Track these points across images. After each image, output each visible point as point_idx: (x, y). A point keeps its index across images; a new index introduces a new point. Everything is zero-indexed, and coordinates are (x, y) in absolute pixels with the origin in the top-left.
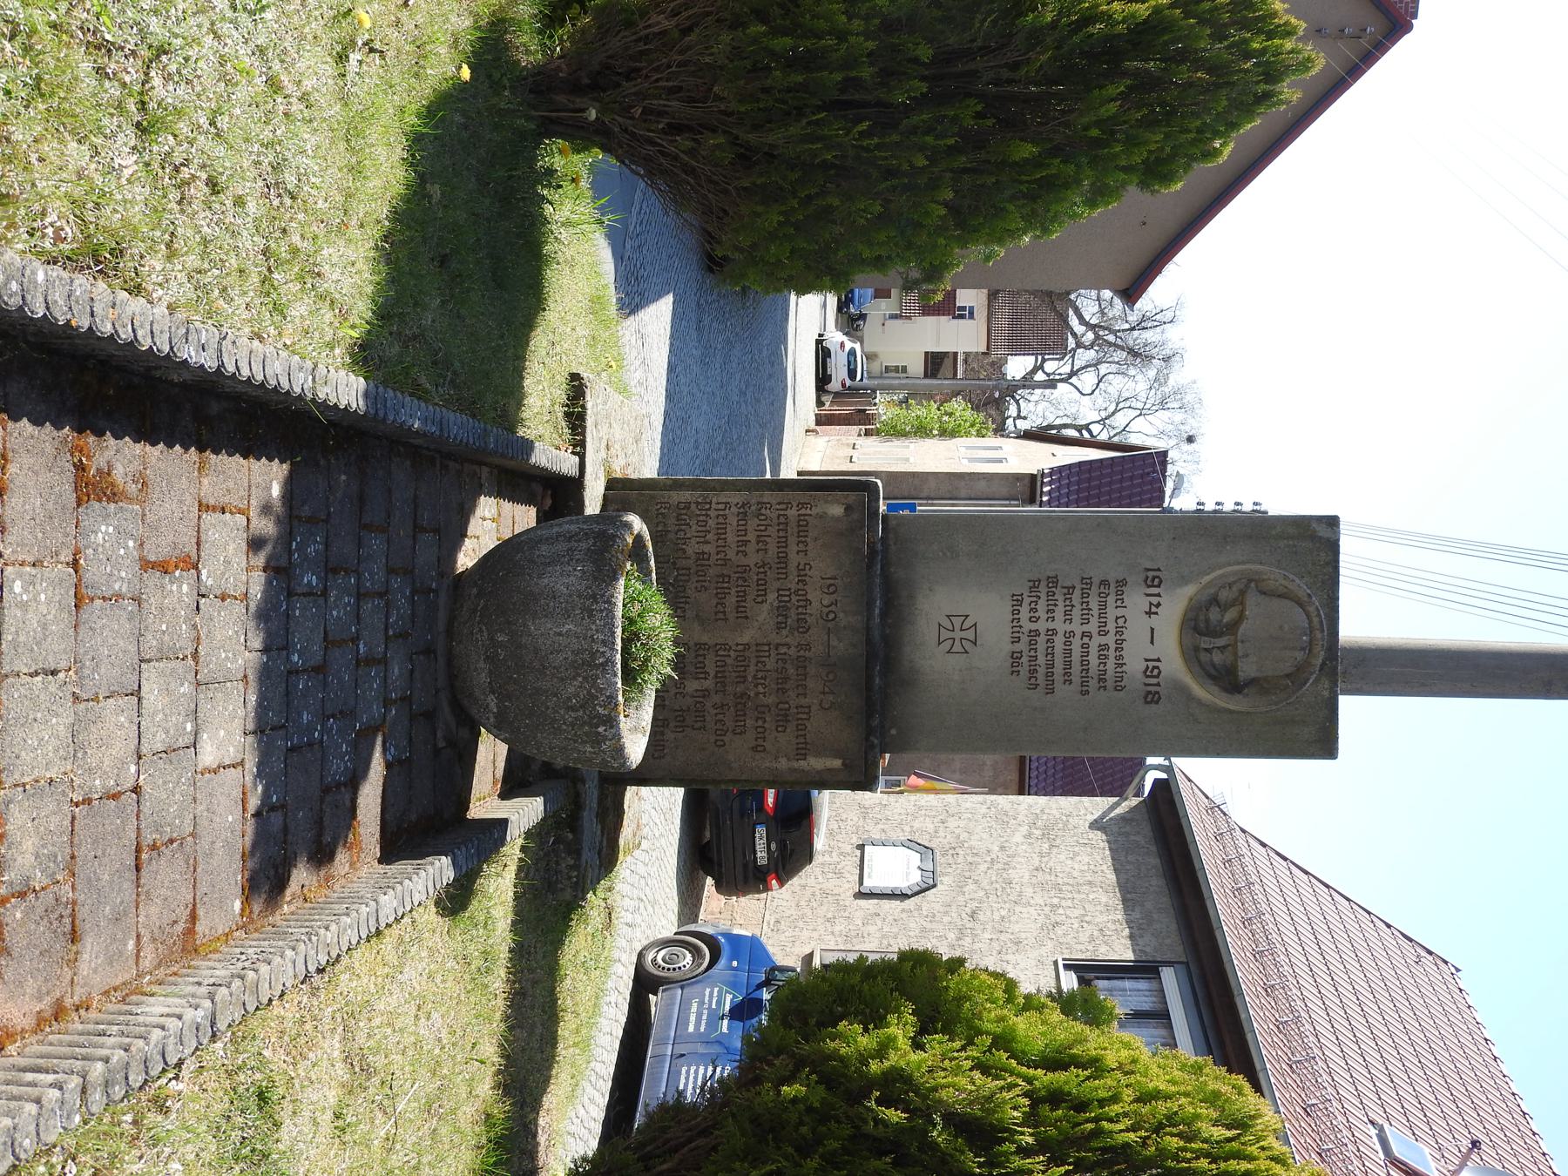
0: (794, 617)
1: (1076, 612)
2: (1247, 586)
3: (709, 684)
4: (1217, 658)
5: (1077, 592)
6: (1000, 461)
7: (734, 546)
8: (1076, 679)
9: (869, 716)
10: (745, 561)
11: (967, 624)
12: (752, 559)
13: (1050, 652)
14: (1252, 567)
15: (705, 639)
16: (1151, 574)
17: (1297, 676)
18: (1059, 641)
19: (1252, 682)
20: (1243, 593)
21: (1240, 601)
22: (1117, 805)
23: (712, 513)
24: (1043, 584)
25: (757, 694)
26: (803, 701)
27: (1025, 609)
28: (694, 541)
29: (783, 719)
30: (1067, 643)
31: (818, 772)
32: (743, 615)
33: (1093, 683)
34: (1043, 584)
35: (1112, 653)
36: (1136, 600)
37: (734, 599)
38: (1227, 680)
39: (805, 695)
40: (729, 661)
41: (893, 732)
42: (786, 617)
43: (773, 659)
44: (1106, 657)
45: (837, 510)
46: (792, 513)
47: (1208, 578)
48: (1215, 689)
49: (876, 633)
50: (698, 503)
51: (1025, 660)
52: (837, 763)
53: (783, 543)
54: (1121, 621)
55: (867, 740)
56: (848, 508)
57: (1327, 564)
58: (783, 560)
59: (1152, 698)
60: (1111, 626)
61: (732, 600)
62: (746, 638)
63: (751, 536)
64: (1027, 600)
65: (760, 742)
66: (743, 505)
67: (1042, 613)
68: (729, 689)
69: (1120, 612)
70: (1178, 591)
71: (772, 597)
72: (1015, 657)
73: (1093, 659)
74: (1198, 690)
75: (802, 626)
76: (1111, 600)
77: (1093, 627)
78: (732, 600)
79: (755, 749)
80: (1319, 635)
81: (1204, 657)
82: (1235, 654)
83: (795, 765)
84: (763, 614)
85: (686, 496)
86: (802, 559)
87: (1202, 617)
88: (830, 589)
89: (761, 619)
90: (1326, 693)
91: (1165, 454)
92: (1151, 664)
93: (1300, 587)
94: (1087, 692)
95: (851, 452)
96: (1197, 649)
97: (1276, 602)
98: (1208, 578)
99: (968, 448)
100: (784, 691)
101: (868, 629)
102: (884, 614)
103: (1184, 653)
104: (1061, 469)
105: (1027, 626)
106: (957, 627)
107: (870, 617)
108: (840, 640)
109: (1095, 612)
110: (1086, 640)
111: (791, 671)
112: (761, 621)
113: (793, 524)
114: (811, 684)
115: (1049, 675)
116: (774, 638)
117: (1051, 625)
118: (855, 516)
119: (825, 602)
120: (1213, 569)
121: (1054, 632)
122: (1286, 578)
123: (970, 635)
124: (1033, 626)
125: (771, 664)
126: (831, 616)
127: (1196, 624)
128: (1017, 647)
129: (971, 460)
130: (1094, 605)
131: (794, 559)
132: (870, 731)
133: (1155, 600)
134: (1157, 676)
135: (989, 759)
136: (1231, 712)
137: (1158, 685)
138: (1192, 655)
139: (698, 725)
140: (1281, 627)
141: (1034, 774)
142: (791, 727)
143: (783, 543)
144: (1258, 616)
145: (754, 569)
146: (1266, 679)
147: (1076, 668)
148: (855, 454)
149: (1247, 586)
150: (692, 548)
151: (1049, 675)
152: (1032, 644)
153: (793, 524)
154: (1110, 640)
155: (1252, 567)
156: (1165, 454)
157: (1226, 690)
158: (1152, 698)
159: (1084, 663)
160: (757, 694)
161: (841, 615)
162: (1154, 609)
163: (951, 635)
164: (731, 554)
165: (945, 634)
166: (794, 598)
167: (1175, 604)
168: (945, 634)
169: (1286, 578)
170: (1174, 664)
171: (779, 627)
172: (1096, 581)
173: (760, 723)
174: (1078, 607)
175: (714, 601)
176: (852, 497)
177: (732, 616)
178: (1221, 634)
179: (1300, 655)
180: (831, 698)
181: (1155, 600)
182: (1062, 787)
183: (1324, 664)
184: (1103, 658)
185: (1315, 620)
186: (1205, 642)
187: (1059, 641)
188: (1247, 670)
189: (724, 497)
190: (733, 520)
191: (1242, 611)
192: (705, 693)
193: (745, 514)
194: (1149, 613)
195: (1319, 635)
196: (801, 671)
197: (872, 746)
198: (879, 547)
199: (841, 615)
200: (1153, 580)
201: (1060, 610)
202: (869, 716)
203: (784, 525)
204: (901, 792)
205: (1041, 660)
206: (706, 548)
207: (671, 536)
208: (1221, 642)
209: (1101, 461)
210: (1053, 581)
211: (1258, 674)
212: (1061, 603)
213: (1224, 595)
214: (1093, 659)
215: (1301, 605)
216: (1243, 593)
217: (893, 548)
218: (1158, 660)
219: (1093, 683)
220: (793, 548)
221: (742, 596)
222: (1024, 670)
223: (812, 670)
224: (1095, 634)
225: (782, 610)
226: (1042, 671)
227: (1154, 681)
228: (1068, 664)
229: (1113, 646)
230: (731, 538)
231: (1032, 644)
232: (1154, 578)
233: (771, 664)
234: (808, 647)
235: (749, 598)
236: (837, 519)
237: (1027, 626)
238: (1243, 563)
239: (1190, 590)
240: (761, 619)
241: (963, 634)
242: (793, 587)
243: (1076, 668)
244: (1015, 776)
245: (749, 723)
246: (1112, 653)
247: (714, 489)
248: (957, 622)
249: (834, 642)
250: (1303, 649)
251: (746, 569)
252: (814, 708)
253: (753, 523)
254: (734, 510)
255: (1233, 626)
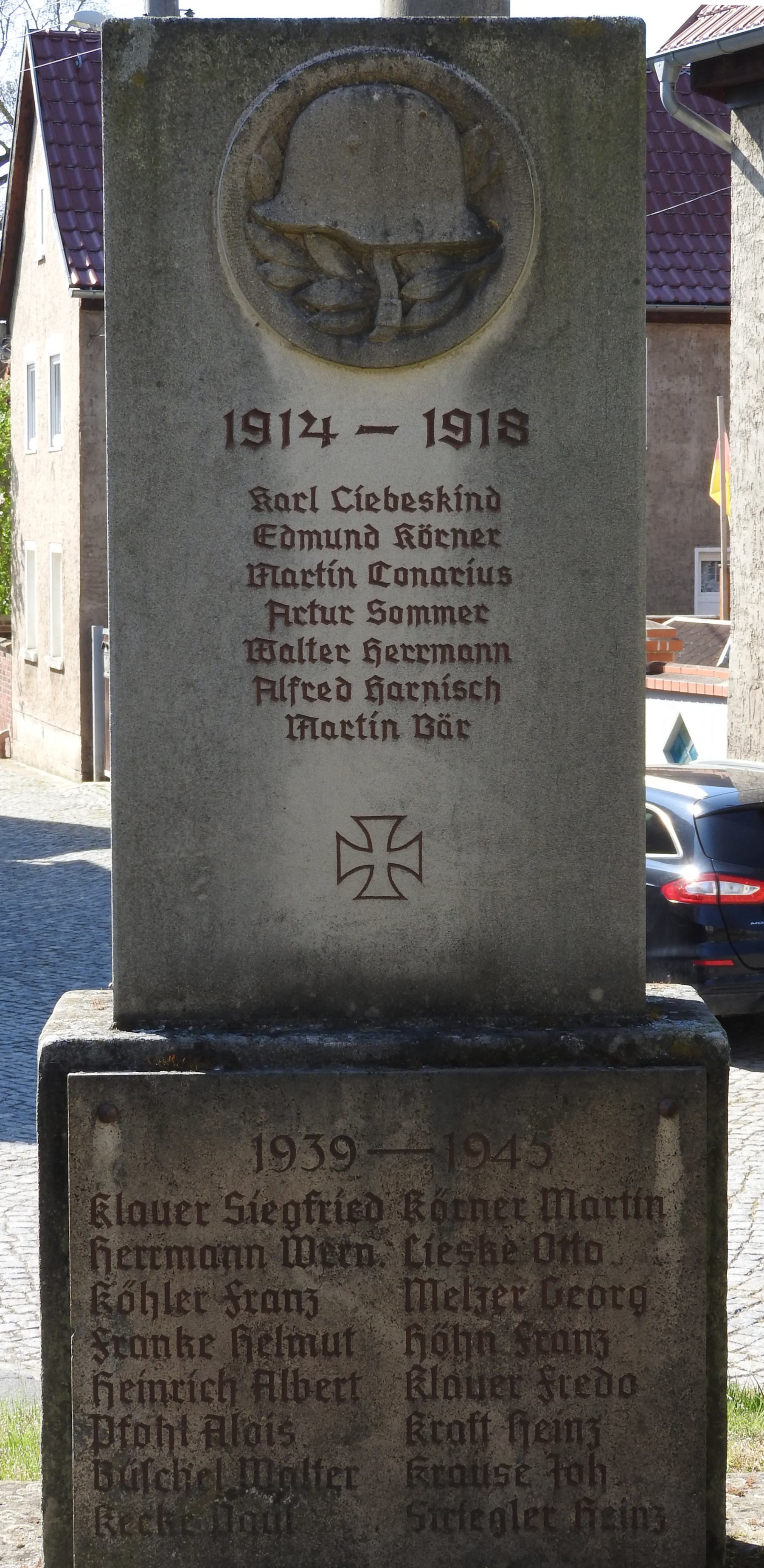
0: (346, 1228)
1: (328, 597)
2: (262, 223)
3: (496, 1414)
4: (423, 288)
5: (283, 596)
6: (56, 371)
7: (190, 1365)
8: (474, 596)
9: (564, 1056)
10: (222, 1344)
11: (354, 835)
12: (219, 1323)
13: (417, 654)
14: (219, 214)
15: (397, 1424)
16: (239, 435)
17: (462, 112)
18: (392, 635)
19: (475, 209)
20: (278, 234)
21: (296, 241)
22: (745, 165)
23: (119, 1413)
24: (264, 671)
25: (517, 1307)
26: (532, 1208)
27: (321, 711)
28: (180, 1453)
29: (573, 1248)
30: (395, 616)
31: (688, 1169)
32: (345, 1340)
33: (484, 558)
34: (264, 671)
35: (417, 519)
36: (298, 466)
37: (309, 1362)
38: (470, 268)
39: (519, 1202)
40: (446, 1369)
41: (597, 995)
42: (346, 1247)
43: (441, 1274)
44: (425, 530)
45: (107, 1139)
46: (114, 1238)
47: (247, 311)
48: (493, 290)
49: (383, 1043)
50: (97, 1446)
51: (433, 710)
52: (668, 1129)
53: (183, 1258)
54: (346, 500)
55: (616, 1062)
56: (102, 1115)
57: (210, 46)
58: (219, 1256)
59: (513, 429)
60: (357, 521)
61: (310, 1367)
62: (391, 1332)
63: (168, 1327)
64: (303, 707)
65: (623, 1298)
66: (100, 1345)
67: (330, 674)
68: (507, 1368)
69: (324, 501)
70: (276, 373)
71: (301, 1279)
72: (428, 730)
73: (432, 558)
74: (496, 328)
75: (365, 1211)
76: (297, 522)
77: (358, 561)
78: (310, 1367)
79: (639, 1310)
80: (369, 65)
81: (420, 318)
82: (414, 249)
83: (672, 1220)
84: (341, 1297)
85: (80, 1470)
86: (216, 1215)
87: (334, 323)
88: (282, 1151)
89: (351, 1302)
90: (499, 46)
91: (38, 38)
92: (440, 432)
93: (263, 106)
94: (504, 571)
95: (42, 671)
96: (404, 334)
97: (298, 161)
98: (247, 311)
99: (31, 433)
100: (511, 1247)
101: (370, 1062)
102: (339, 1022)
103: (415, 360)
104: (70, 249)
105: (359, 704)
106: (363, 859)
107: (344, 1059)
108: (396, 1127)
109: (326, 556)
110: (387, 576)
111: (466, 1233)
112: (362, 1304)
113: (140, 1235)
114: (493, 1191)
115: (465, 655)
116: (393, 1273)
117: (356, 653)
118: (120, 1098)
119: (312, 1161)
120: (228, 298)
121: (372, 645)
122: (242, 139)
123: (380, 830)
124: (359, 691)
125: (450, 1278)
126: (343, 1147)
127: (350, 334)
128: (406, 726)
129: (55, 427)
130: (309, 559)
131: (216, 1231)
132: (597, 1054)
133: (297, 425)
134: (466, 417)
135: (651, 385)
136: (543, 254)
137: (484, 415)
138: (417, 343)
139: (588, 1435)
140: (353, 149)
141: (685, 294)
142: (591, 1231)
143: (183, 1258)
144: (330, 199)
145: (242, 1318)
146: (468, 180)
147: (452, 596)
148: (47, 662)
149: (262, 223)
150: (197, 1456)
151: (465, 655)
152: (398, 694)
153: (140, 1235)
154: (386, 523)
155: (219, 214)
156: (38, 38)
157: (495, 268)
158: (513, 429)
159: (440, 578)
160: (517, 1307)
161: (340, 1125)
162: (317, 427)
163: (380, 874)
164: (209, 1370)
165: (380, 885)
166: (304, 1230)
167: (306, 381)
168: (380, 885)
169: (242, 139)
170: (439, 382)
171: (368, 1262)
172: (257, 555)
173: (582, 1299)
174: (314, 594)
175: (313, 1404)
176: (77, 1107)
177: (345, 1366)
178: (370, 277)
179: (415, 108)
180: (524, 1145)
181: (297, 425)
182: (711, 237)
183: (435, 54)
184: (428, 538)
185: (336, 72)
186: (389, 315)
187: (392, 635)
188: (448, 222)
189: (82, 1389)
190: (133, 1367)
191: (319, 234)
192: (518, 1420)
193: (118, 1341)
194: (327, 437)
195: (369, 65)
196: (465, 1212)
197: (630, 1047)
198: (187, 1040)
199: (340, 1125)
200: (253, 430)
201: (324, 635)
202: (564, 1056)
203: (141, 1255)
204: (727, 562)
205: (433, 673)
206: (196, 1425)
207: (170, 1503)
208: (387, 279)
209: (53, 167)
210: (258, 650)
211: (459, 199)
212: (308, 632)
213: (284, 273)
214: (432, 558)
215: (303, 105)
216: (278, 234)
217: (190, 1002)
218: (430, 416)
219: (484, 558)
220: (194, 1234)
221: (301, 1343)
222: (458, 711)
223: (463, 1188)
224: (374, 556)
225: (332, 1256)
226: (457, 672)
227: (476, 425)
228: (442, 614)
229: (401, 517)
230: (173, 1370)
231: (398, 694)
232: (247, 427)
233: (450, 1278)
234: (412, 1197)
235: (306, 1328)
236: (128, 1138)
237: (359, 704)
238: (211, 232)
239: (275, 350)
240: (351, 1302)
241: (380, 845)
242: (278, 1232)
243: (452, 596)
244: (691, 333)
245: (581, 1322)
246: (417, 519)
247: (65, 1406)
248: (351, 859)
249: (400, 1141)
250: (401, 100)
251: (240, 1336)
252: (546, 1181)
253: (139, 1324)
254: (109, 1365)
255: (354, 255)
